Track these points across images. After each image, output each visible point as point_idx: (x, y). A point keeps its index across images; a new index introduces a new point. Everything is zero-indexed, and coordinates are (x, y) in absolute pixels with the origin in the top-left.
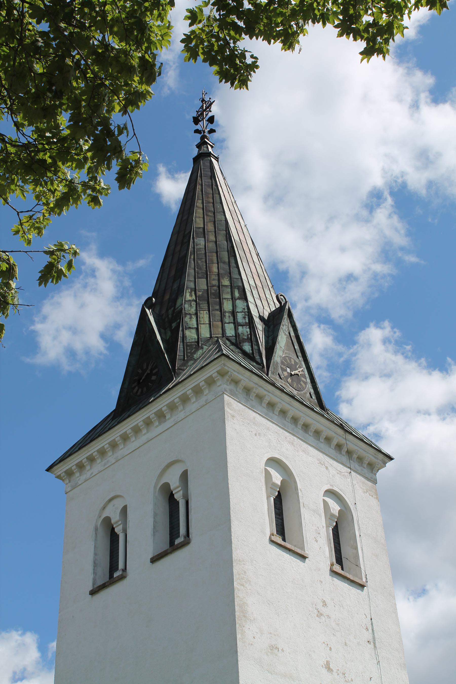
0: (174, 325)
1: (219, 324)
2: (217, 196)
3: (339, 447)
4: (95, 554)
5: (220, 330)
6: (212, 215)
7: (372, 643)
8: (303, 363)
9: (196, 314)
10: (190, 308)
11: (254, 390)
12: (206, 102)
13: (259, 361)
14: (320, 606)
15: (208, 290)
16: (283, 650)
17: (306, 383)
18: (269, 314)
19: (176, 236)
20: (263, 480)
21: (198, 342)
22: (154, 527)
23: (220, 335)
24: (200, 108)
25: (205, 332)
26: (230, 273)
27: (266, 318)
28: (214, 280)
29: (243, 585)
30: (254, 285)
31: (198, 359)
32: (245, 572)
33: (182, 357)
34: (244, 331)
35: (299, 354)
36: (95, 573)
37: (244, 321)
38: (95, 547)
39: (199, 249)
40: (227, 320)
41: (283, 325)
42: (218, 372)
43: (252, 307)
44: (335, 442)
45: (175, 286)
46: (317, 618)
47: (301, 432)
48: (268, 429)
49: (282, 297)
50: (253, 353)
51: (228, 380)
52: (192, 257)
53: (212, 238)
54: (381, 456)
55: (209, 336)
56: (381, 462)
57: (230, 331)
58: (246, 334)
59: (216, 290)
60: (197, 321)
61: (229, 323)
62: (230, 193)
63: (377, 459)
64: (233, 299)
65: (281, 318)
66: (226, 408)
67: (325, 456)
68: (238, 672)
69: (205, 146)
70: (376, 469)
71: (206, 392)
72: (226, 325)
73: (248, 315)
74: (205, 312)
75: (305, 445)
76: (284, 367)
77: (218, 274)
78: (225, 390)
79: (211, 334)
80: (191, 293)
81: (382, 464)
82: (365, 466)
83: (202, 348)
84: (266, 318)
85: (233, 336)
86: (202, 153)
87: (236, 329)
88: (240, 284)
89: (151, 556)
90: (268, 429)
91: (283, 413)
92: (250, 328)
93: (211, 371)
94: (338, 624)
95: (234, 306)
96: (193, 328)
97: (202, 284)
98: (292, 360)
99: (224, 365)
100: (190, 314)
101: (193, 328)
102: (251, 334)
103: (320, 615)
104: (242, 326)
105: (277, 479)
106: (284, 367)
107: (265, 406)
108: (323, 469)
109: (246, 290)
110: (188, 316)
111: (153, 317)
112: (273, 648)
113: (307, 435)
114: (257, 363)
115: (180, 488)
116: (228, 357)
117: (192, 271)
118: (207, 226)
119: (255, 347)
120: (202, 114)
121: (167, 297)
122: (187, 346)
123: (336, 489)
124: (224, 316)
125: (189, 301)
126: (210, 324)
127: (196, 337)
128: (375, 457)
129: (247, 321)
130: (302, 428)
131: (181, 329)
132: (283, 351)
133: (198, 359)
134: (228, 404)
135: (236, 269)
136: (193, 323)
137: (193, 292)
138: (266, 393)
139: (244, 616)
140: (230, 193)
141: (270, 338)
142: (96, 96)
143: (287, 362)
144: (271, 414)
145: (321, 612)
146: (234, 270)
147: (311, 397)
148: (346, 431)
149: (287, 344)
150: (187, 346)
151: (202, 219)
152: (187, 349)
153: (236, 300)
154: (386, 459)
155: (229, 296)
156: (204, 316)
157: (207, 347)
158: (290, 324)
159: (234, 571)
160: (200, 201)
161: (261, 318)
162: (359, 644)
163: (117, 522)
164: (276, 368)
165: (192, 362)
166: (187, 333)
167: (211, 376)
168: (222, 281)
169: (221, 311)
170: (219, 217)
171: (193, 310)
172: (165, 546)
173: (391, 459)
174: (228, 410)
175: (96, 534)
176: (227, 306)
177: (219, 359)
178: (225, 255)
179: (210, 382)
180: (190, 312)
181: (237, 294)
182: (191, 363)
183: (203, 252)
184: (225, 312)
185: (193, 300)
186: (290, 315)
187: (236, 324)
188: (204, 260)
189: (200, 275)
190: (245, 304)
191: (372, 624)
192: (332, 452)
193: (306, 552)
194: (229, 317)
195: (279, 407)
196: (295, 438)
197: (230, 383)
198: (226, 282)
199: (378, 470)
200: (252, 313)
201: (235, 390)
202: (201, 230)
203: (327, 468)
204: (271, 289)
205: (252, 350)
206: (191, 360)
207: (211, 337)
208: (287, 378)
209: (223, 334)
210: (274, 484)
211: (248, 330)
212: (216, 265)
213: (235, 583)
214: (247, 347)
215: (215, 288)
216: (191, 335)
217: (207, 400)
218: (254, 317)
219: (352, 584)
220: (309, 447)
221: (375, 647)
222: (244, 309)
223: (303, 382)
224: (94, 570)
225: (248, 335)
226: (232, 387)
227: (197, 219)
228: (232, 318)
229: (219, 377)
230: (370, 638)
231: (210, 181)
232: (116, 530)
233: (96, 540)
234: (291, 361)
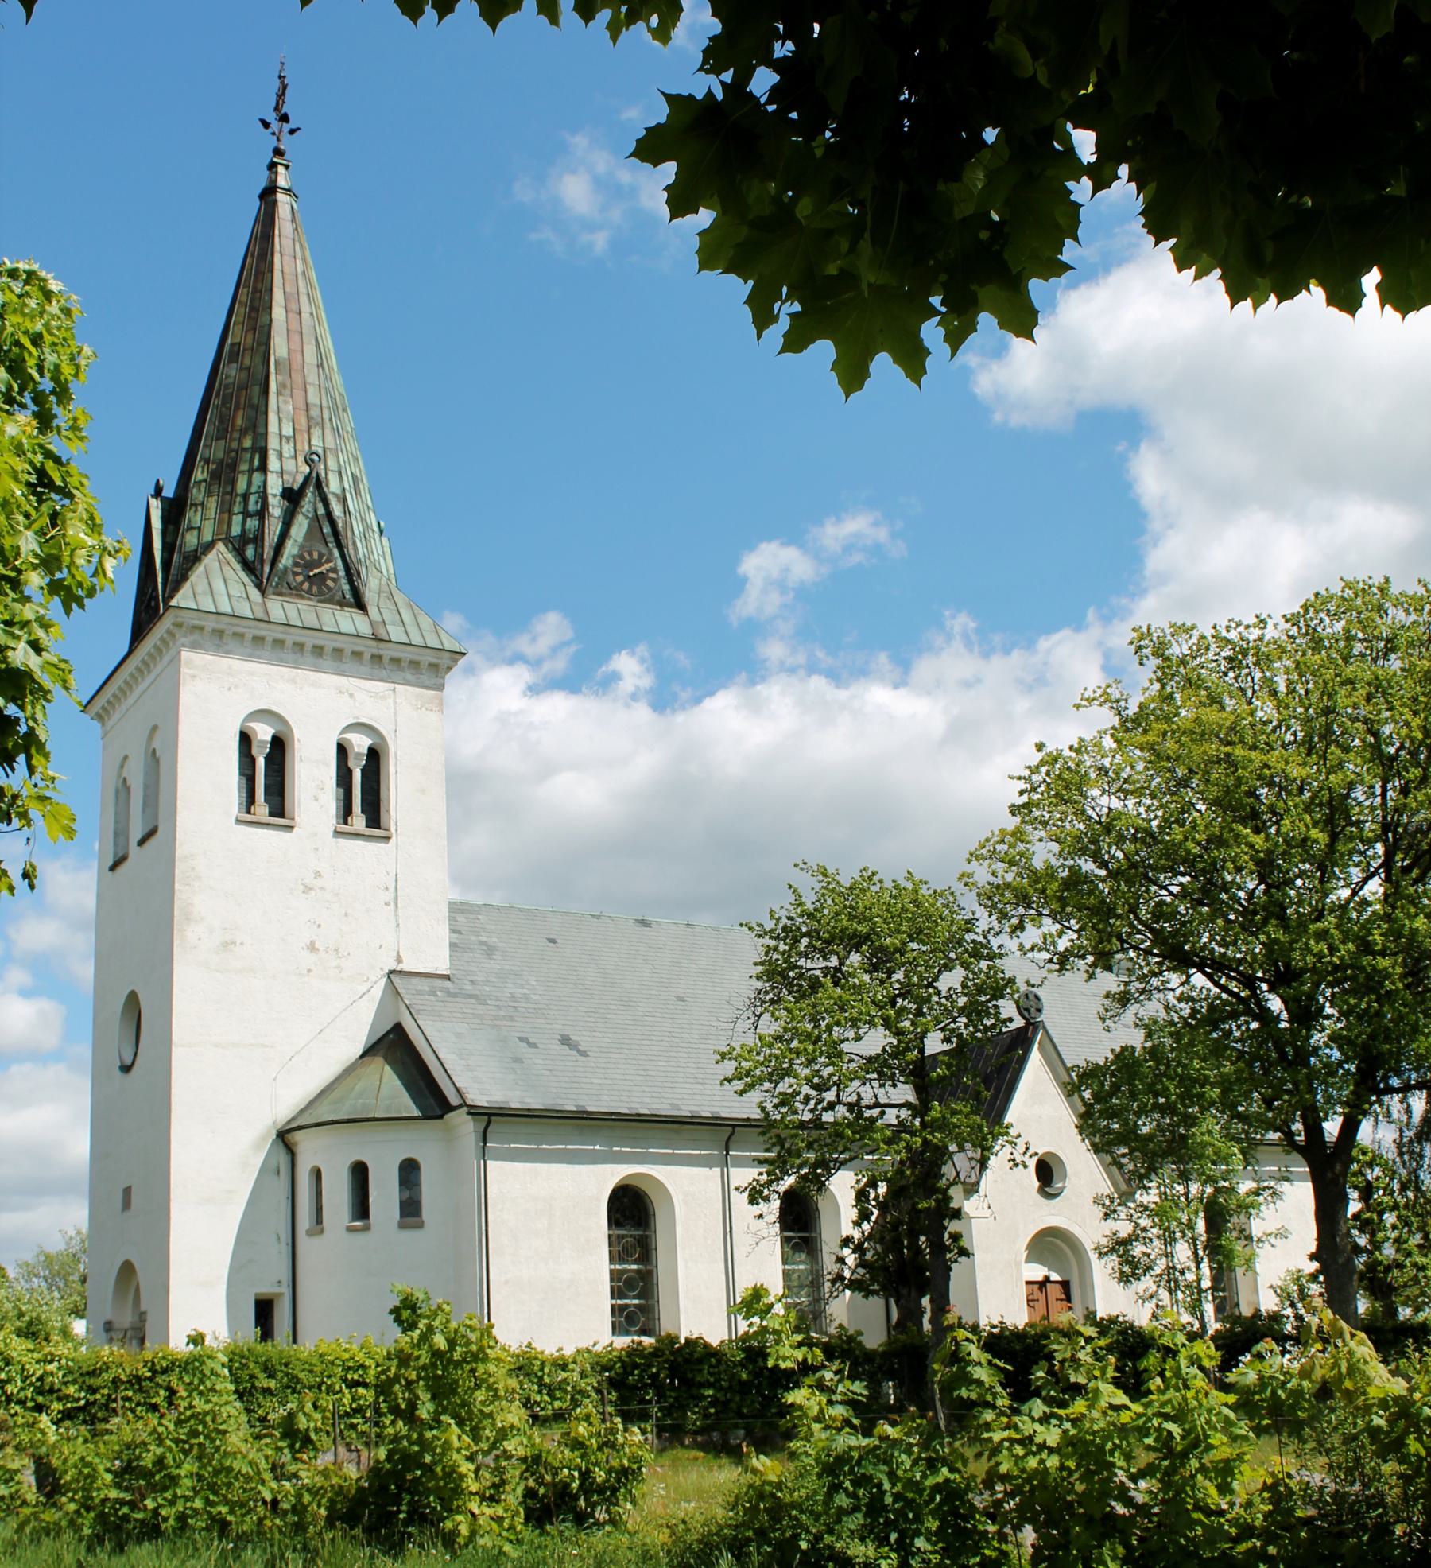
4: (116, 822)
9: (202, 504)
35: (331, 539)
53: (247, 362)
54: (447, 655)
103: (307, 889)
112: (227, 945)
146: (261, 419)
156: (213, 505)
176: (241, 485)
178: (256, 390)
187: (246, 514)
203: (351, 695)
210: (264, 742)
223: (333, 580)
230: (390, 896)
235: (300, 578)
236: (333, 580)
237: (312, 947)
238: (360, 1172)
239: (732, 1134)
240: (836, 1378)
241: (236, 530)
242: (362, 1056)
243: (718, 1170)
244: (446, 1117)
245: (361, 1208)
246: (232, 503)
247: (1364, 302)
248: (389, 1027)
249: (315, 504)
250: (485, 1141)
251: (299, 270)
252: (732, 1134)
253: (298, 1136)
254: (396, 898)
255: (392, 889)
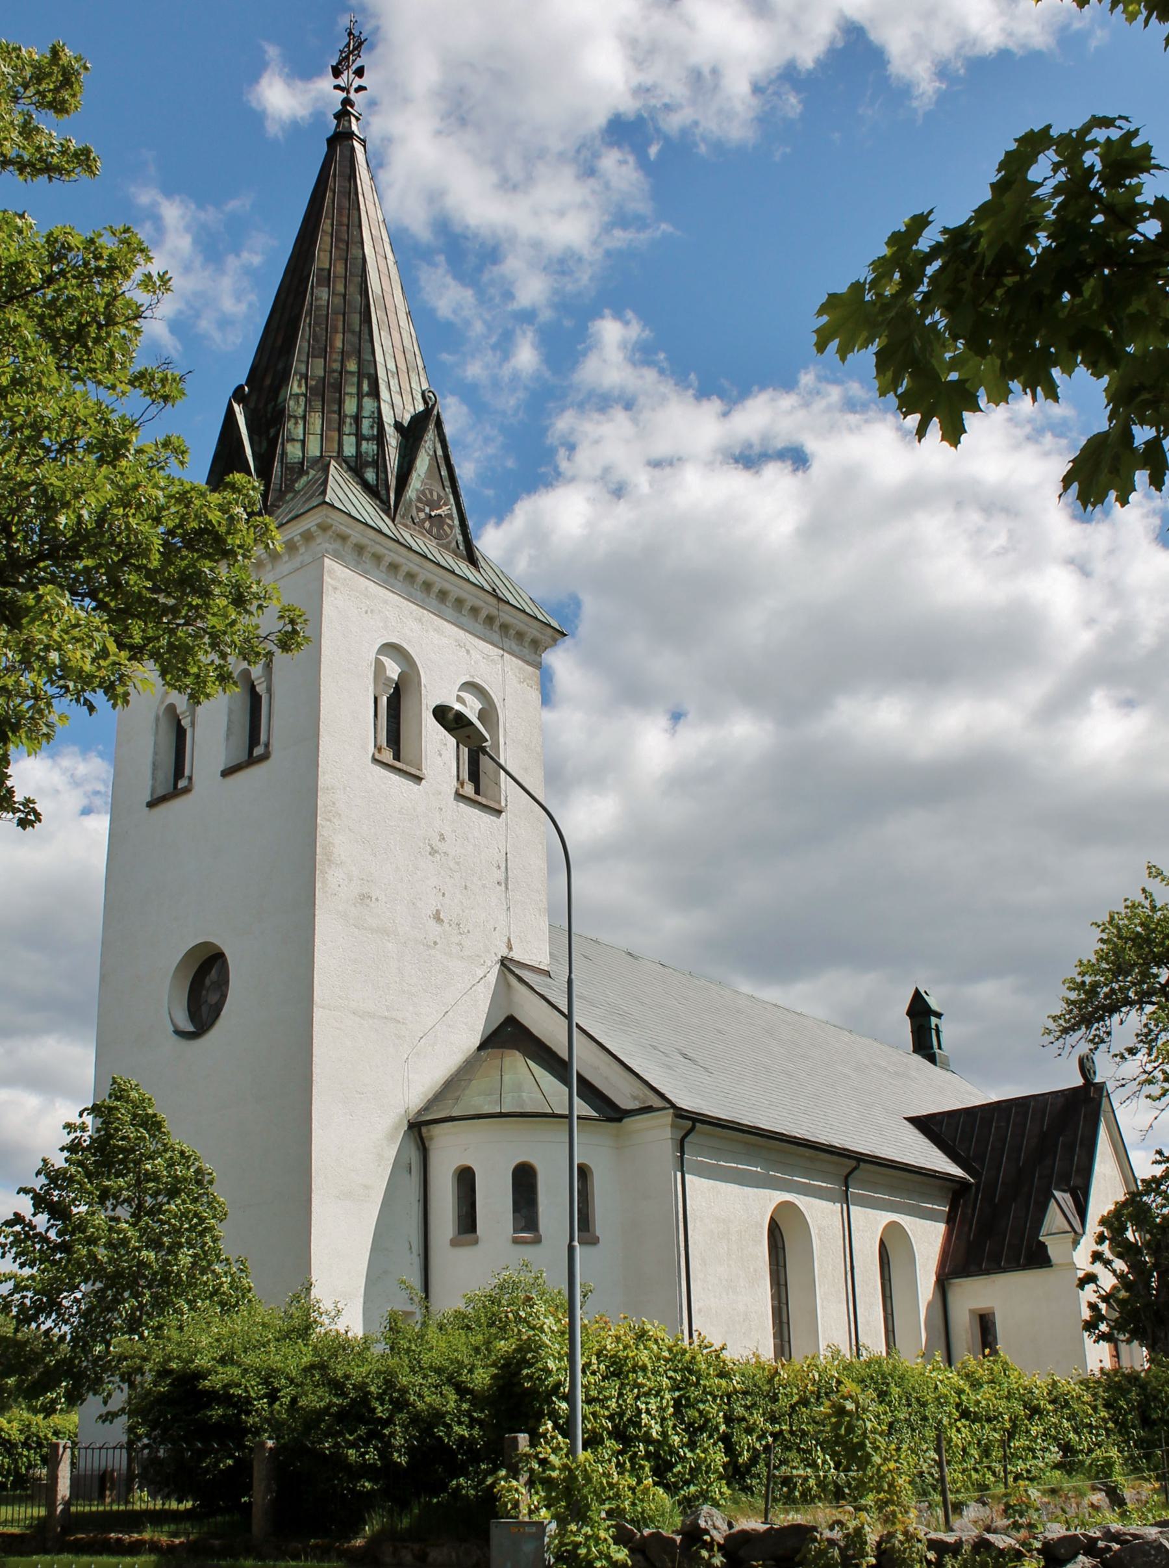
1: (335, 435)
2: (355, 212)
3: (490, 620)
4: (155, 753)
5: (336, 446)
6: (345, 247)
7: (503, 885)
8: (451, 497)
9: (304, 418)
10: (296, 407)
11: (369, 549)
12: (354, 37)
13: (384, 498)
14: (436, 842)
15: (325, 377)
16: (377, 899)
17: (451, 527)
18: (412, 417)
20: (371, 676)
21: (302, 463)
22: (229, 729)
23: (335, 454)
24: (345, 47)
25: (314, 450)
26: (359, 352)
27: (406, 425)
28: (335, 361)
29: (329, 820)
30: (395, 370)
31: (299, 491)
32: (334, 803)
33: (278, 486)
34: (369, 448)
35: (447, 483)
36: (154, 779)
37: (371, 433)
38: (155, 744)
39: (318, 308)
41: (426, 442)
42: (319, 526)
44: (483, 614)
45: (280, 366)
46: (430, 857)
47: (435, 602)
48: (386, 602)
49: (431, 395)
50: (377, 485)
51: (331, 537)
52: (308, 321)
53: (340, 288)
54: (550, 631)
55: (319, 455)
56: (550, 640)
58: (371, 454)
59: (335, 379)
61: (349, 435)
62: (377, 205)
63: (544, 635)
64: (360, 396)
65: (424, 430)
66: (326, 578)
67: (467, 634)
68: (314, 929)
69: (346, 118)
70: (542, 648)
71: (302, 550)
72: (345, 437)
73: (378, 424)
74: (317, 414)
75: (438, 621)
76: (421, 506)
77: (343, 352)
78: (327, 552)
80: (300, 381)
81: (551, 642)
82: (526, 645)
83: (308, 473)
84: (406, 425)
85: (353, 456)
86: (340, 133)
87: (358, 445)
88: (372, 372)
90: (386, 602)
91: (411, 577)
92: (378, 444)
94: (458, 863)
95: (360, 407)
96: (297, 440)
97: (318, 368)
98: (435, 494)
99: (327, 516)
100: (296, 417)
101: (297, 440)
102: (378, 454)
103: (434, 852)
104: (368, 440)
105: (393, 670)
106: (421, 506)
107: (384, 570)
108: (463, 653)
109: (380, 381)
110: (293, 421)
111: (245, 416)
112: (364, 898)
113: (444, 607)
114: (382, 501)
115: (263, 679)
116: (332, 506)
117: (305, 345)
118: (335, 267)
119: (382, 476)
120: (347, 58)
121: (268, 382)
122: (286, 468)
123: (477, 680)
124: (344, 423)
125: (297, 395)
126: (322, 435)
127: (301, 455)
128: (541, 633)
129: (375, 433)
130: (437, 596)
131: (280, 441)
132: (422, 482)
133: (299, 491)
134: (329, 572)
135: (369, 345)
137: (303, 381)
138: (386, 552)
139: (328, 860)
140: (377, 205)
141: (407, 459)
144: (392, 581)
145: (436, 848)
146: (366, 346)
147: (458, 548)
148: (500, 599)
149: (429, 469)
151: (328, 254)
152: (286, 474)
153: (363, 397)
154: (557, 636)
155: (354, 390)
156: (316, 421)
157: (314, 472)
158: (437, 438)
159: (319, 802)
160: (329, 221)
161: (398, 426)
162: (484, 886)
163: (183, 713)
164: (408, 509)
166: (289, 447)
168: (348, 364)
169: (340, 414)
170: (354, 251)
171: (300, 411)
172: (243, 756)
174: (329, 580)
175: (157, 725)
176: (350, 407)
177: (320, 508)
178: (356, 319)
179: (308, 537)
180: (296, 414)
181: (365, 388)
182: (289, 496)
183: (325, 313)
184: (346, 416)
185: (303, 394)
186: (439, 424)
187: (360, 437)
188: (324, 326)
189: (316, 353)
190: (376, 404)
191: (506, 860)
192: (479, 627)
193: (424, 771)
194: (351, 424)
195: (404, 569)
196: (425, 612)
197: (335, 540)
198: (352, 366)
199: (546, 648)
200: (385, 419)
201: (341, 549)
202: (325, 273)
203: (468, 652)
204: (422, 372)
206: (291, 492)
207: (321, 456)
208: (423, 521)
209: (339, 452)
210: (389, 679)
211: (375, 447)
212: (341, 335)
213: (319, 818)
214: (370, 475)
215: (336, 375)
216: (294, 451)
218: (386, 426)
219: (485, 809)
220: (445, 623)
221: (507, 888)
222: (373, 412)
223: (449, 526)
224: (153, 774)
225: (373, 456)
226: (337, 545)
227: (322, 254)
228: (354, 426)
229: (319, 532)
230: (502, 878)
231: (348, 185)
232: (183, 723)
233: (156, 733)
235: (422, 515)
236: (449, 526)
237: (438, 918)
238: (466, 1179)
239: (854, 1169)
241: (349, 450)
242: (481, 1047)
243: (839, 1205)
244: (625, 1120)
245: (467, 1223)
246: (341, 423)
248: (502, 1019)
249: (434, 443)
250: (682, 1152)
251: (381, 219)
252: (854, 1169)
253: (437, 1130)
254: (507, 879)
255: (503, 869)
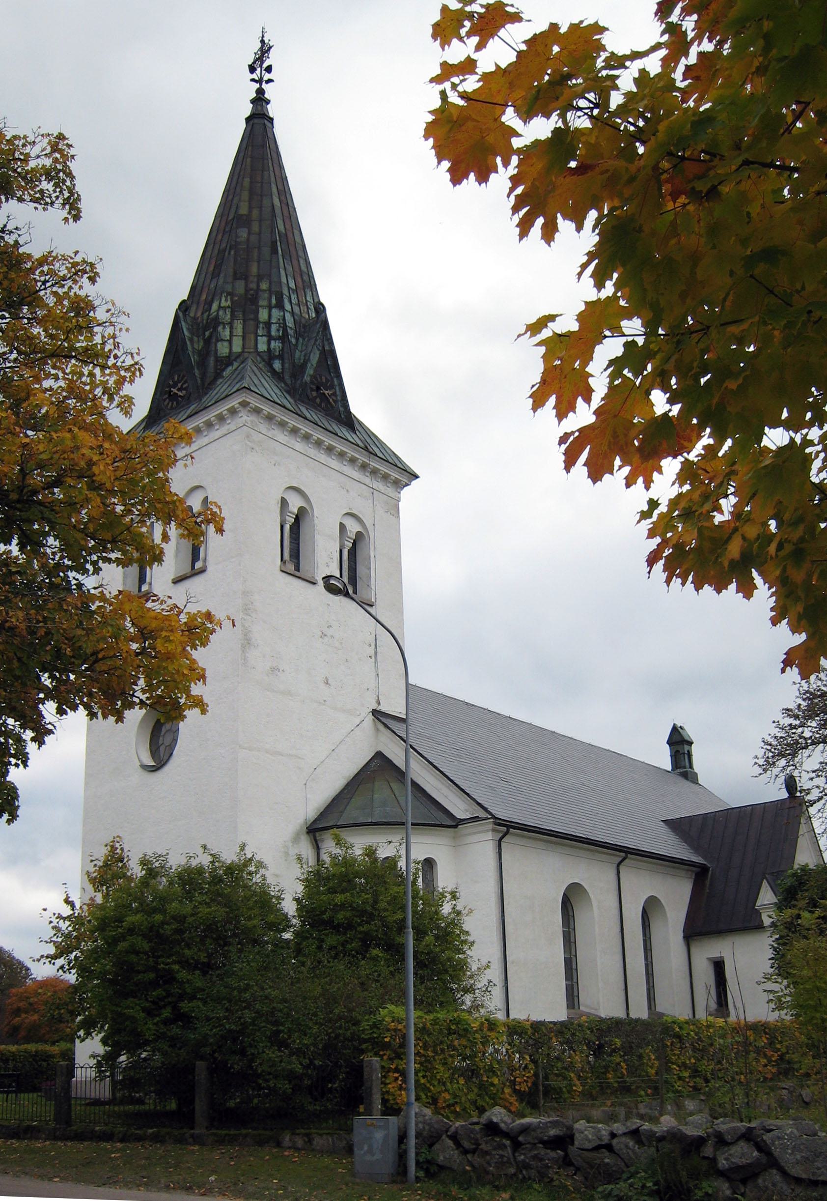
0: (207, 334)
7: (373, 658)
16: (283, 671)
19: (219, 219)
37: (277, 334)
40: (260, 332)
43: (288, 317)
50: (283, 373)
57: (262, 347)
60: (231, 332)
72: (259, 338)
74: (239, 321)
79: (244, 347)
80: (226, 297)
85: (264, 351)
87: (269, 344)
89: (172, 576)
93: (234, 402)
96: (224, 340)
98: (323, 378)
101: (224, 340)
112: (274, 670)
123: (354, 511)
136: (227, 333)
142: (73, 317)
143: (317, 380)
150: (218, 359)
165: (221, 380)
167: (234, 406)
172: (187, 569)
173: (417, 477)
176: (263, 315)
179: (233, 412)
184: (260, 322)
185: (229, 307)
187: (270, 338)
205: (282, 369)
207: (243, 352)
217: (229, 429)
222: (279, 319)
228: (265, 330)
230: (371, 651)
234: (321, 380)
240: (680, 1064)
247: (533, 140)
254: (376, 653)
255: (373, 646)
